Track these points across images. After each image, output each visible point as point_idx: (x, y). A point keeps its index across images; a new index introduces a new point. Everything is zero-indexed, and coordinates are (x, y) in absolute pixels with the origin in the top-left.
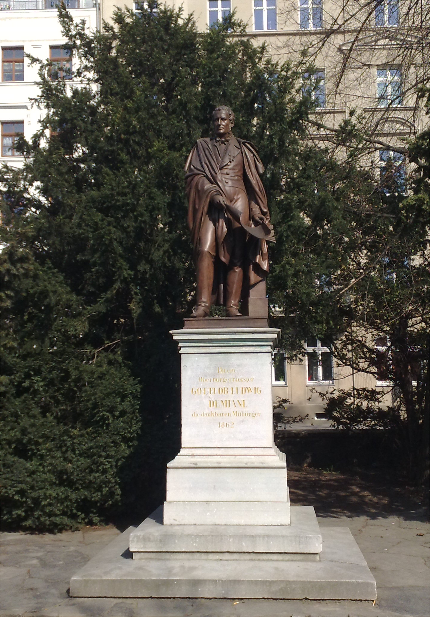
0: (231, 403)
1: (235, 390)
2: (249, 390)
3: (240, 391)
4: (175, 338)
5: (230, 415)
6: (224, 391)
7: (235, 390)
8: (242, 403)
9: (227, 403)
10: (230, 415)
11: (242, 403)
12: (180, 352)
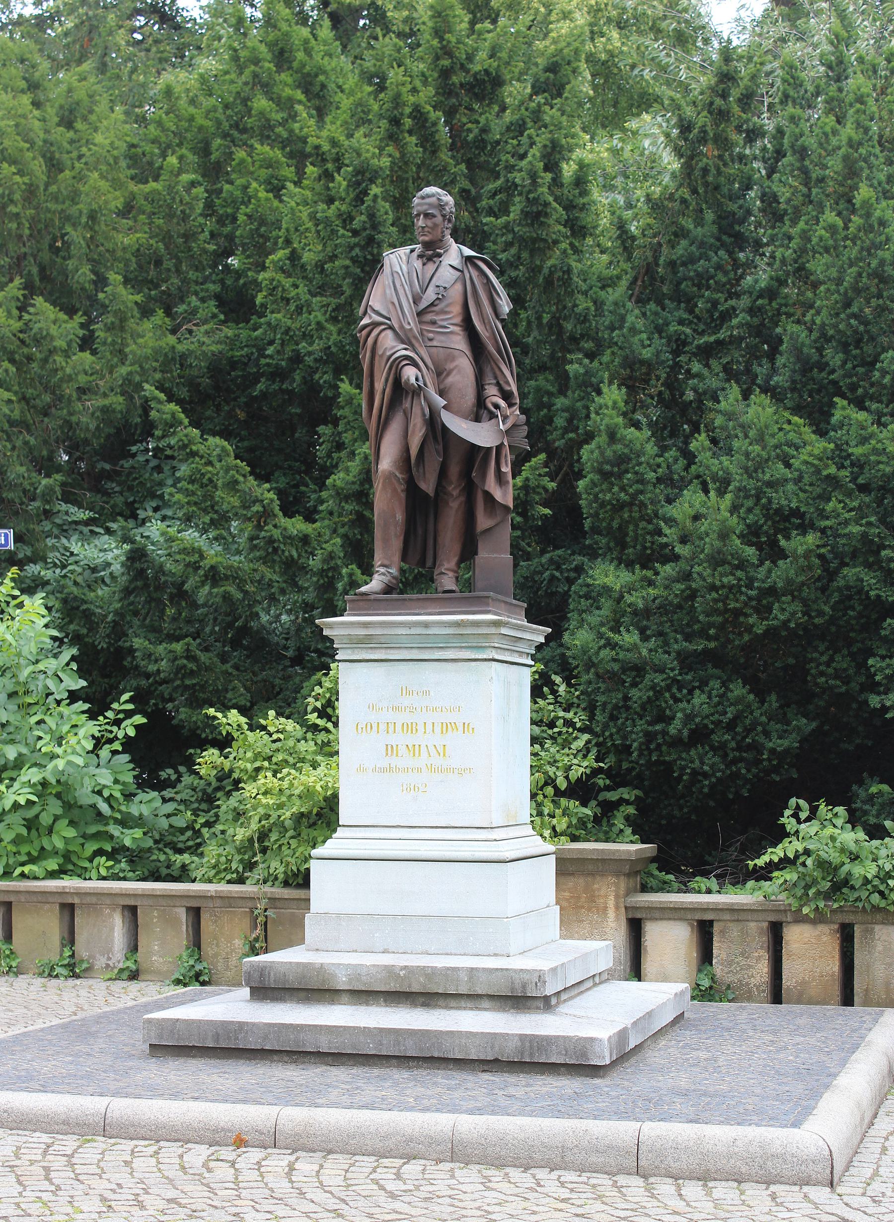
0: (423, 748)
1: (429, 727)
3: (438, 729)
5: (419, 770)
6: (410, 728)
7: (429, 727)
8: (441, 750)
9: (414, 750)
10: (419, 770)
11: (441, 750)
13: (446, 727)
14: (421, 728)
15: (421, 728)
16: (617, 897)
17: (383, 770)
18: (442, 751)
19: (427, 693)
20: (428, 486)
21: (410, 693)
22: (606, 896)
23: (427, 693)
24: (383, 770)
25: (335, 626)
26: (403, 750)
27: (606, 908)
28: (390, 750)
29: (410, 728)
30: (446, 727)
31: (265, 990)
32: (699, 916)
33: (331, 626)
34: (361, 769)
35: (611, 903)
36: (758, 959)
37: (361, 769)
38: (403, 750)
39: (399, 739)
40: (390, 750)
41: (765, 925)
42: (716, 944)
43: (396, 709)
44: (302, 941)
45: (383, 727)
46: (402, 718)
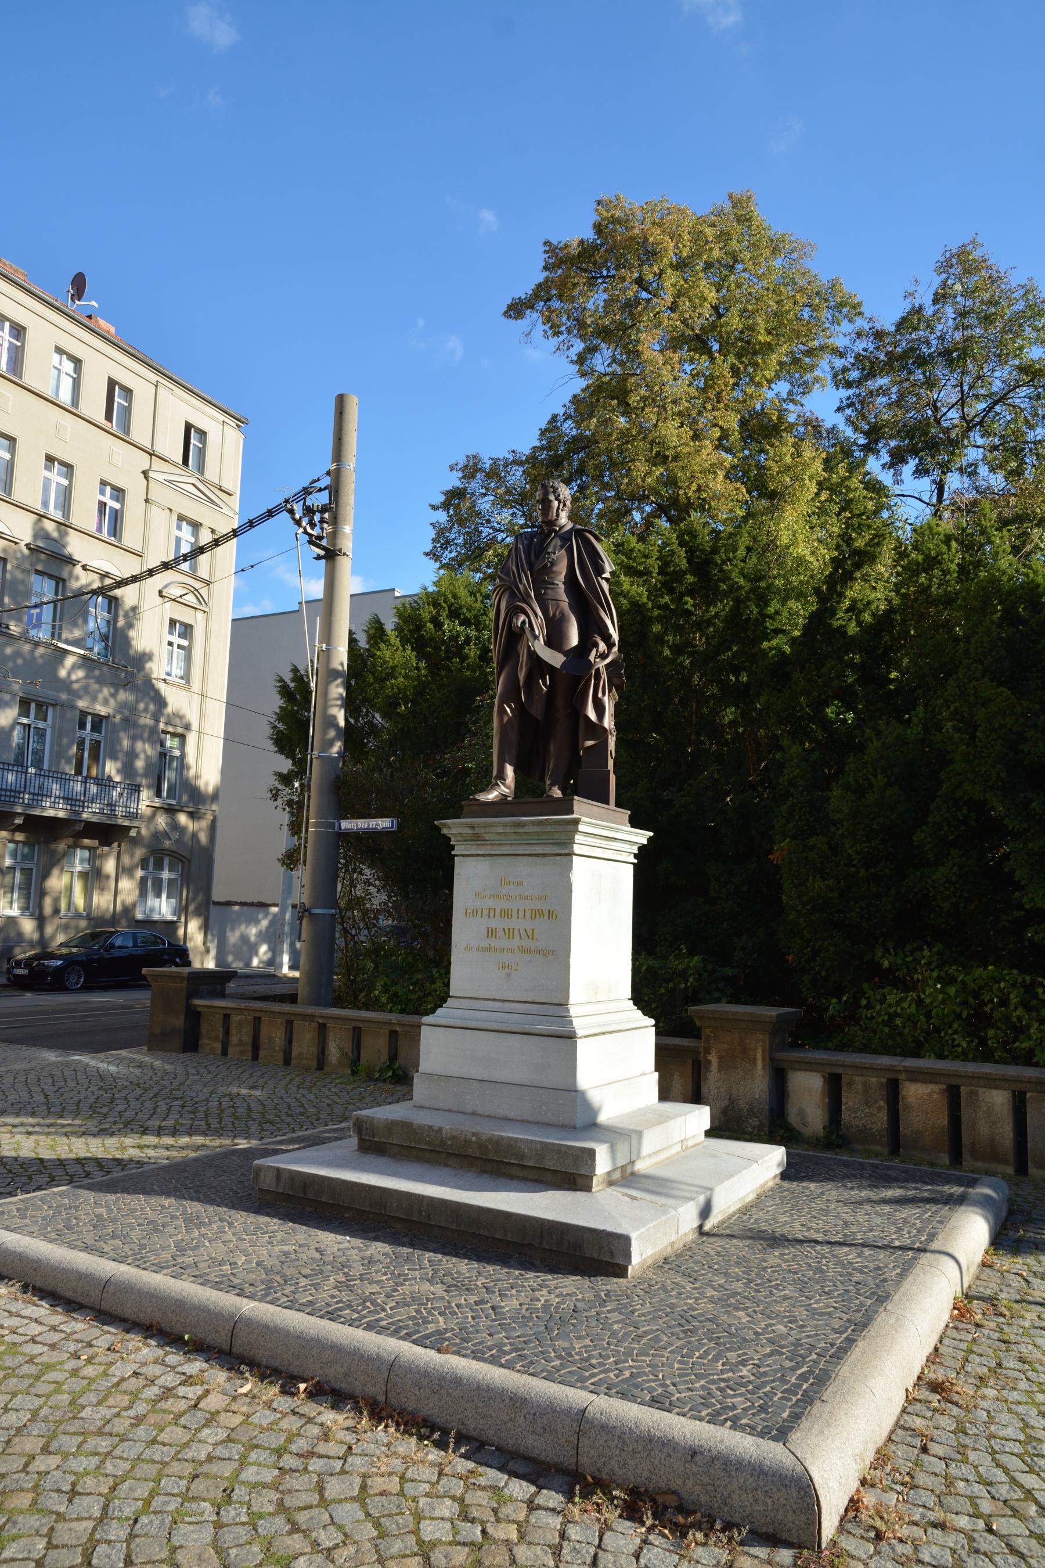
1: (521, 913)
2: (541, 913)
3: (528, 914)
4: (445, 831)
5: (512, 951)
6: (506, 914)
7: (521, 913)
9: (509, 933)
10: (512, 951)
13: (536, 914)
14: (515, 914)
15: (515, 914)
16: (763, 1051)
17: (484, 950)
18: (531, 935)
19: (520, 884)
20: (537, 711)
22: (756, 1049)
23: (520, 884)
24: (484, 950)
25: (453, 828)
26: (500, 933)
27: (755, 1059)
28: (491, 933)
29: (506, 914)
30: (536, 914)
31: (375, 1145)
32: (829, 1070)
33: (445, 825)
34: (468, 948)
35: (759, 1055)
36: (880, 1109)
37: (468, 948)
38: (500, 933)
39: (497, 923)
40: (491, 933)
41: (884, 1080)
42: (844, 1094)
43: (496, 896)
44: (408, 1096)
45: (485, 912)
46: (500, 905)
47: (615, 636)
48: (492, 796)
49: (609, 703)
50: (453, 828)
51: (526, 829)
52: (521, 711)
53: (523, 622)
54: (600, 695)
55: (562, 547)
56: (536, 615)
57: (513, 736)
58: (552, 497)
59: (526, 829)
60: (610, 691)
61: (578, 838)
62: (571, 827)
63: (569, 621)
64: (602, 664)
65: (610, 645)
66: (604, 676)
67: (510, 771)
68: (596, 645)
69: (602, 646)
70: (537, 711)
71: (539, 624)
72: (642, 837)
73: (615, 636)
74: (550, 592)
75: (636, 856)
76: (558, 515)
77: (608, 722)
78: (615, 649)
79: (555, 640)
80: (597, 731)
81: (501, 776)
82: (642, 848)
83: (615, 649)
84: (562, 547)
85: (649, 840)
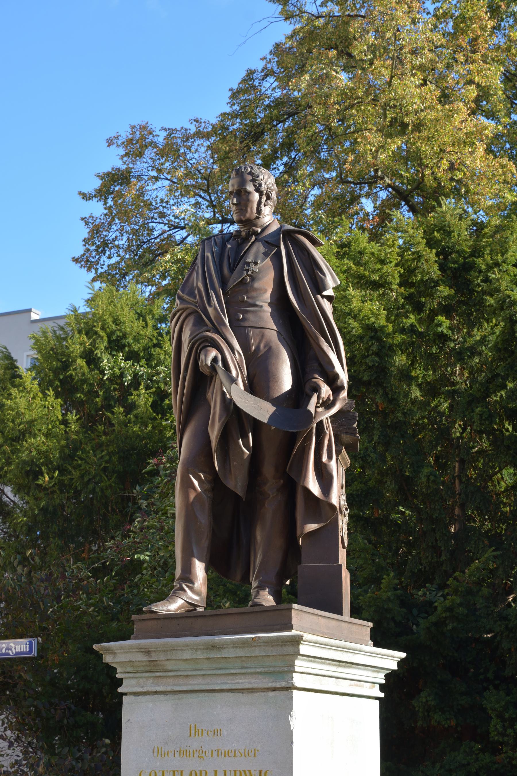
4: (107, 659)
12: (120, 690)
19: (218, 733)
20: (237, 483)
21: (199, 733)
25: (118, 654)
43: (183, 753)
47: (344, 377)
48: (175, 606)
49: (337, 469)
50: (118, 654)
51: (225, 653)
52: (216, 484)
53: (215, 360)
54: (325, 459)
55: (266, 254)
56: (232, 349)
57: (204, 519)
58: (250, 188)
59: (225, 653)
60: (338, 453)
61: (299, 664)
62: (289, 649)
63: (278, 356)
64: (325, 416)
65: (336, 389)
66: (330, 432)
67: (199, 569)
68: (317, 389)
69: (326, 391)
70: (237, 483)
71: (236, 361)
72: (391, 659)
73: (344, 377)
74: (250, 316)
75: (382, 687)
76: (259, 211)
77: (337, 497)
78: (344, 394)
79: (258, 382)
80: (320, 508)
81: (188, 577)
82: (390, 676)
83: (344, 394)
84: (266, 254)
85: (401, 663)
